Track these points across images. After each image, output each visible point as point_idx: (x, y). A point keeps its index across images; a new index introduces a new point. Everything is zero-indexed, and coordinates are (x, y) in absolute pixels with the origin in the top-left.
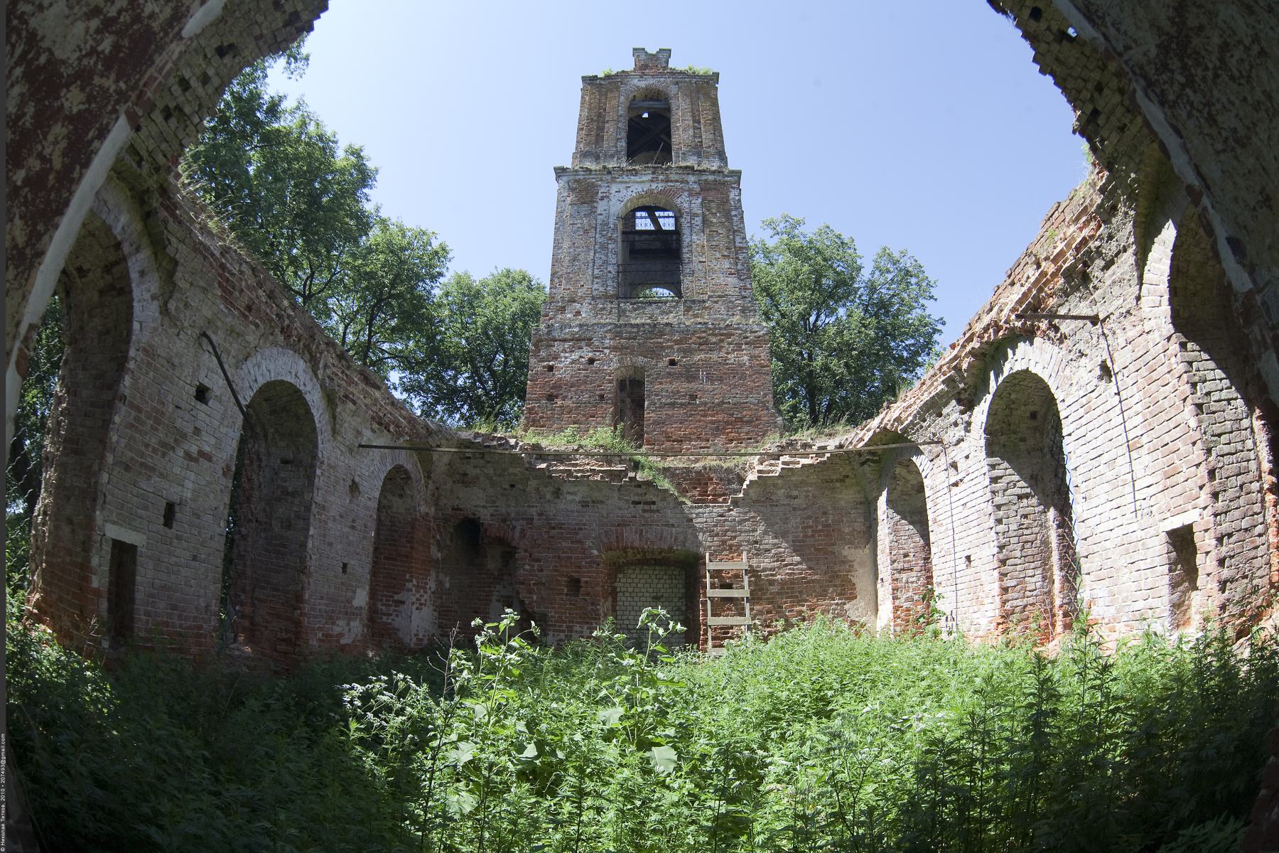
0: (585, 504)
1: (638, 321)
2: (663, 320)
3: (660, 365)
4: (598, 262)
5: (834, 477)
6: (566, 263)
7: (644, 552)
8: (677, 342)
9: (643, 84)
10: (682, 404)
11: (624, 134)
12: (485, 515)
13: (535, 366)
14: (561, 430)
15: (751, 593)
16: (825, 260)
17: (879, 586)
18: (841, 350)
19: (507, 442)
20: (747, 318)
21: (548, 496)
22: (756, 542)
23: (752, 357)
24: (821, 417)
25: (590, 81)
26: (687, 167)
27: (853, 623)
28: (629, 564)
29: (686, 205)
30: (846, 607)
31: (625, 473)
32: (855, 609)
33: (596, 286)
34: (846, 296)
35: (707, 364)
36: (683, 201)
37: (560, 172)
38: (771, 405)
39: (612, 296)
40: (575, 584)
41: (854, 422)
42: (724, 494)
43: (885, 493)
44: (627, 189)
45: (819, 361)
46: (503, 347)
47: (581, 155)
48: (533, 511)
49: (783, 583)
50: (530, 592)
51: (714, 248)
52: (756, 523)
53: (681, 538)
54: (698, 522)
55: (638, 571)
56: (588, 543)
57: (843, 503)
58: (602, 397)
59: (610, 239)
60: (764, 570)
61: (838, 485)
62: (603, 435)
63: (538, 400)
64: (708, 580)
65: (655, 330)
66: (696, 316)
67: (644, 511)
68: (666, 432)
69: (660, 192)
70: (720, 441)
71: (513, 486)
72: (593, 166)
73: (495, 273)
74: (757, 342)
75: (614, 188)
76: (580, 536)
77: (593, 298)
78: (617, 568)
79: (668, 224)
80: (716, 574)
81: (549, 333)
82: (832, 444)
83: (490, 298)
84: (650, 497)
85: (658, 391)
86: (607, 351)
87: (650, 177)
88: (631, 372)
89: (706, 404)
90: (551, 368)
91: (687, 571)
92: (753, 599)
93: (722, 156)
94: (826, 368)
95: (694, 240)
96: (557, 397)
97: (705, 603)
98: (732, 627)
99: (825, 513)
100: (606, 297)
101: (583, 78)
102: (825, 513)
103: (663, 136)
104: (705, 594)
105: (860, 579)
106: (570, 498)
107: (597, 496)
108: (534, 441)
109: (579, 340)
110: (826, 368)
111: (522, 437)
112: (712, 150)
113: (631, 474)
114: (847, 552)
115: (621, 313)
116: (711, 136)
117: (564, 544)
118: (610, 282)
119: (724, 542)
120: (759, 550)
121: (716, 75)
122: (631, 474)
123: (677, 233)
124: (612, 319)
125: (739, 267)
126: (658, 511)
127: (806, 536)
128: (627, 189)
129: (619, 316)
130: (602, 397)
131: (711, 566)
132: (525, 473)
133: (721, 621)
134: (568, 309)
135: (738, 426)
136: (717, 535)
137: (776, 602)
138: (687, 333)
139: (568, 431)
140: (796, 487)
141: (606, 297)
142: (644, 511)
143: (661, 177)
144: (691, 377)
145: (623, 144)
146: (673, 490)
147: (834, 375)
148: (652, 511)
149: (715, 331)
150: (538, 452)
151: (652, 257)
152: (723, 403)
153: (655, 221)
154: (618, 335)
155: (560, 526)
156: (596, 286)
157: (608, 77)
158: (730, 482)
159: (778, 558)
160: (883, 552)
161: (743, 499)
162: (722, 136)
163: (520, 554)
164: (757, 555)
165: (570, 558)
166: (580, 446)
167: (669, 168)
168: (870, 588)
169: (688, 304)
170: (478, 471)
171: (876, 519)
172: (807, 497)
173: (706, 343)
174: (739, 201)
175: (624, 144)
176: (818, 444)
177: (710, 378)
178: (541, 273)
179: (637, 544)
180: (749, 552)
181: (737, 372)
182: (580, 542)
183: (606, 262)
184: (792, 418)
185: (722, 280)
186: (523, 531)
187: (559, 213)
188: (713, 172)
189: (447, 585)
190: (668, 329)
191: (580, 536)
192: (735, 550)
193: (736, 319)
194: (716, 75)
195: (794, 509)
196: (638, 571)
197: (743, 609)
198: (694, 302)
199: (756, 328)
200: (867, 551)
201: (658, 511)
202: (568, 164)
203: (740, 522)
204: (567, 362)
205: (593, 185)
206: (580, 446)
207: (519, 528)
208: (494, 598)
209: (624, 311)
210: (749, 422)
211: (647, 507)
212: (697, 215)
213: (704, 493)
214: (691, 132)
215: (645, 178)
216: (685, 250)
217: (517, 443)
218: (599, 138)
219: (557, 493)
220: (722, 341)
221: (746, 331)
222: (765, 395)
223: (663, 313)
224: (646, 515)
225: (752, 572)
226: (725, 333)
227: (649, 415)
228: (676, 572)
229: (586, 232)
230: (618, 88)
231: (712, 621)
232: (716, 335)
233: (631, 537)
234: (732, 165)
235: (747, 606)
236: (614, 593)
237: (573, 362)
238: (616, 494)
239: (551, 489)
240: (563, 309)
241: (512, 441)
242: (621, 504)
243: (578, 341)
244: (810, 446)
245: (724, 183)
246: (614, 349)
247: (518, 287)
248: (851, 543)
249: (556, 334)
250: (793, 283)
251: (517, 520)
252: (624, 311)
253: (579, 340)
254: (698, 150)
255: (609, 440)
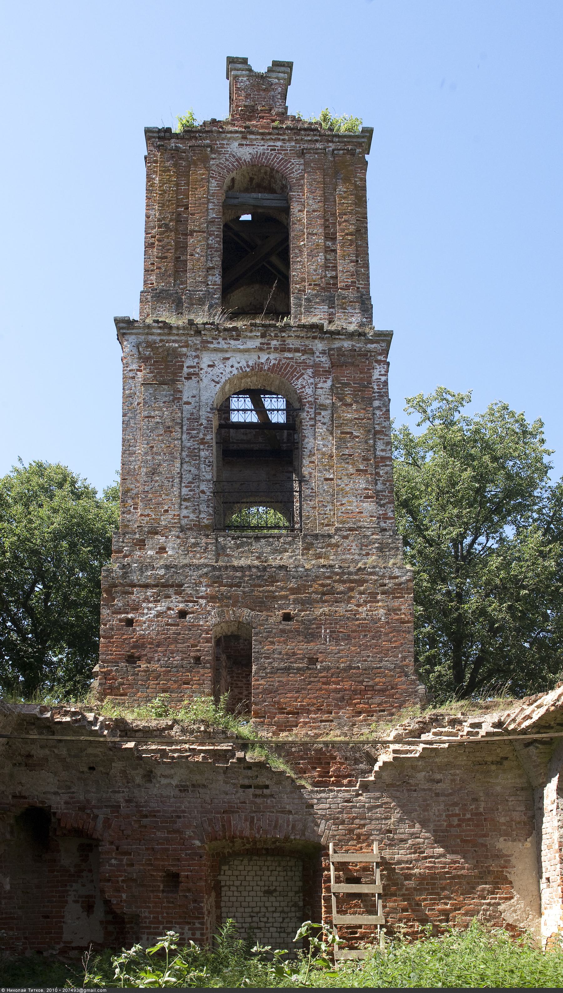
0: (183, 789)
1: (243, 562)
2: (275, 561)
3: (271, 620)
4: (188, 477)
5: (490, 759)
6: (143, 477)
7: (255, 842)
8: (293, 591)
9: (245, 153)
10: (299, 669)
11: (217, 260)
12: (58, 803)
13: (109, 619)
14: (148, 700)
15: (385, 887)
16: (495, 459)
17: (543, 885)
18: (504, 590)
19: (84, 717)
20: (385, 558)
21: (138, 780)
22: (389, 831)
23: (390, 611)
24: (470, 682)
25: (158, 138)
26: (313, 327)
27: (510, 927)
28: (236, 854)
29: (309, 391)
30: (501, 908)
31: (230, 754)
32: (513, 909)
33: (185, 512)
34: (521, 508)
35: (332, 620)
36: (305, 385)
37: (124, 326)
38: (411, 669)
39: (207, 526)
40: (173, 879)
41: (518, 692)
42: (350, 776)
43: (555, 781)
44: (220, 368)
45: (473, 602)
46: (40, 576)
47: (154, 296)
48: (120, 797)
49: (422, 878)
50: (118, 890)
51: (346, 458)
52: (390, 810)
53: (300, 826)
54: (320, 809)
55: (245, 862)
56: (189, 833)
57: (498, 789)
58: (197, 659)
59: (202, 442)
60: (399, 862)
61: (493, 767)
62: (199, 708)
63: (115, 662)
64: (332, 873)
65: (266, 575)
66: (318, 556)
67: (255, 796)
68: (279, 703)
69: (272, 369)
70: (345, 713)
71: (92, 769)
72: (173, 320)
73: (20, 466)
74: (397, 591)
75: (206, 359)
76: (179, 824)
77: (182, 529)
78: (220, 860)
79: (276, 409)
80: (341, 866)
81: (125, 575)
82: (488, 722)
83: (19, 508)
84: (263, 780)
85: (268, 653)
86: (203, 602)
87: (257, 343)
88: (234, 628)
89: (328, 669)
90: (130, 623)
91: (309, 859)
92: (385, 895)
93: (365, 306)
94: (482, 612)
95: (318, 442)
96: (139, 658)
97: (328, 900)
98: (360, 927)
99: (475, 800)
100: (199, 528)
101: (148, 131)
102: (475, 800)
103: (274, 259)
104: (328, 889)
105: (519, 872)
106: (164, 781)
107: (198, 778)
108: (115, 714)
109: (165, 586)
110: (482, 612)
111: (100, 710)
112: (351, 294)
113: (240, 754)
114: (502, 844)
115: (220, 551)
116: (351, 267)
117: (159, 834)
118: (203, 507)
119: (351, 831)
120: (393, 839)
121: (368, 133)
122: (240, 754)
123: (292, 425)
124: (208, 559)
125: (380, 487)
126: (272, 796)
127: (450, 826)
128: (220, 368)
129: (218, 555)
130: (197, 659)
131: (335, 856)
132: (108, 757)
133: (349, 919)
134: (149, 543)
135: (371, 696)
136: (343, 823)
137: (415, 901)
138: (306, 579)
139: (157, 702)
140: (441, 769)
141: (199, 528)
142: (255, 796)
143: (274, 343)
144: (311, 635)
145: (216, 279)
146: (290, 773)
147: (492, 622)
148: (264, 796)
149: (343, 575)
150: (122, 728)
151: (257, 462)
152: (350, 667)
153: (259, 408)
154: (216, 581)
155: (153, 814)
156: (185, 512)
157: (190, 132)
158: (357, 761)
159: (416, 849)
160: (549, 847)
161: (374, 782)
162: (366, 266)
163: (105, 847)
164: (390, 845)
165: (167, 850)
166: (175, 721)
167: (288, 326)
168: (533, 888)
169: (309, 539)
170: (47, 752)
171: (541, 809)
172: (453, 780)
173: (331, 592)
174: (386, 383)
175: (218, 279)
176: (470, 721)
177: (335, 637)
178: (99, 467)
179: (247, 833)
180: (380, 841)
181: (370, 628)
182: (178, 831)
183: (197, 478)
184: (428, 672)
185: (353, 504)
186: (107, 821)
187: (128, 398)
188: (351, 335)
189: (8, 887)
190: (282, 573)
191: (179, 824)
192: (364, 840)
193: (372, 559)
194: (368, 133)
195: (437, 795)
196: (245, 862)
197: (374, 905)
198: (316, 536)
199: (397, 572)
200: (528, 844)
201: (272, 796)
202: (133, 313)
203: (370, 809)
204: (152, 614)
205: (175, 354)
206: (175, 721)
207: (101, 817)
208: (70, 899)
209: (224, 548)
210: (383, 691)
211: (259, 792)
212: (323, 407)
213: (325, 774)
214: (320, 259)
215: (253, 344)
216: (305, 462)
217: (96, 719)
218: (179, 267)
219: (149, 776)
220: (351, 589)
221: (383, 577)
222: (404, 658)
223: (275, 551)
224: (258, 800)
225: (384, 864)
226: (355, 579)
227: (258, 682)
228: (291, 863)
229: (168, 430)
230: (205, 160)
231: (337, 918)
232: (344, 582)
233: (239, 824)
234: (380, 323)
235: (380, 903)
236: (217, 888)
237: (159, 615)
238: (221, 778)
239: (141, 771)
240: (141, 544)
241: (90, 716)
242: (228, 788)
243: (166, 587)
244: (460, 722)
245: (366, 355)
246: (211, 598)
247: (58, 492)
248: (507, 834)
249: (135, 577)
250: (448, 492)
251: (98, 808)
252: (224, 548)
253: (165, 586)
254: (329, 293)
255: (211, 714)
